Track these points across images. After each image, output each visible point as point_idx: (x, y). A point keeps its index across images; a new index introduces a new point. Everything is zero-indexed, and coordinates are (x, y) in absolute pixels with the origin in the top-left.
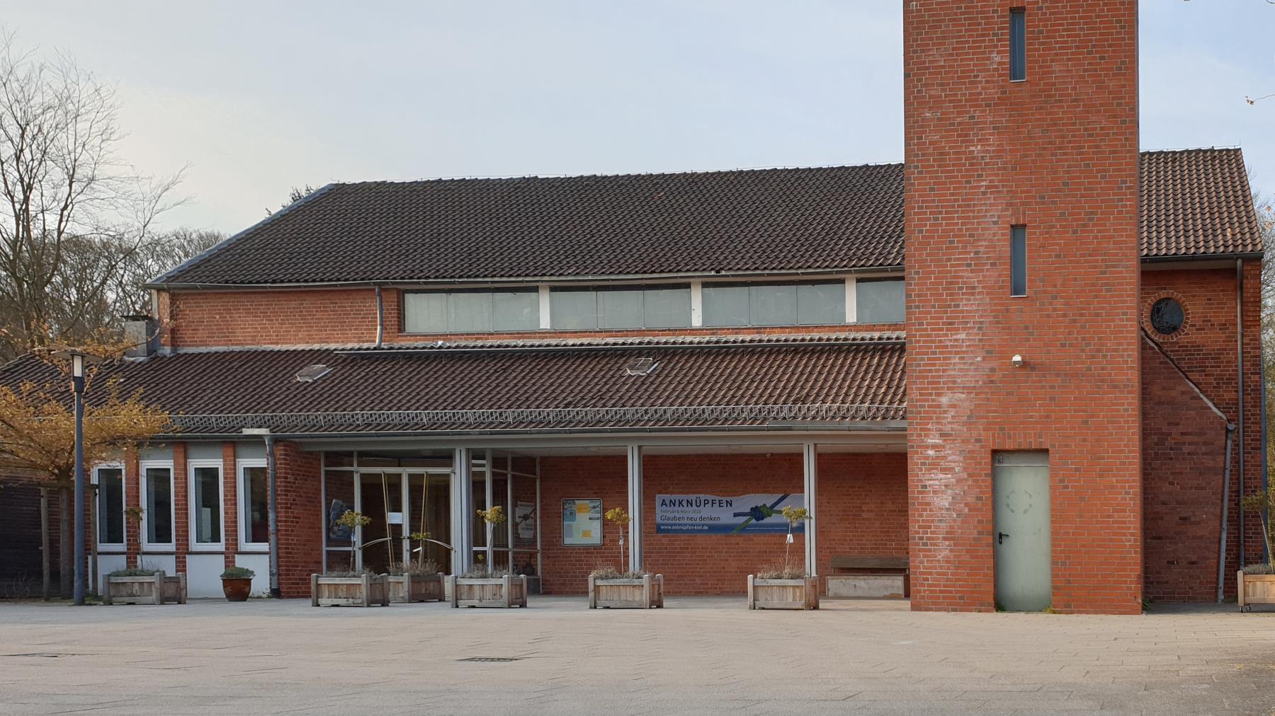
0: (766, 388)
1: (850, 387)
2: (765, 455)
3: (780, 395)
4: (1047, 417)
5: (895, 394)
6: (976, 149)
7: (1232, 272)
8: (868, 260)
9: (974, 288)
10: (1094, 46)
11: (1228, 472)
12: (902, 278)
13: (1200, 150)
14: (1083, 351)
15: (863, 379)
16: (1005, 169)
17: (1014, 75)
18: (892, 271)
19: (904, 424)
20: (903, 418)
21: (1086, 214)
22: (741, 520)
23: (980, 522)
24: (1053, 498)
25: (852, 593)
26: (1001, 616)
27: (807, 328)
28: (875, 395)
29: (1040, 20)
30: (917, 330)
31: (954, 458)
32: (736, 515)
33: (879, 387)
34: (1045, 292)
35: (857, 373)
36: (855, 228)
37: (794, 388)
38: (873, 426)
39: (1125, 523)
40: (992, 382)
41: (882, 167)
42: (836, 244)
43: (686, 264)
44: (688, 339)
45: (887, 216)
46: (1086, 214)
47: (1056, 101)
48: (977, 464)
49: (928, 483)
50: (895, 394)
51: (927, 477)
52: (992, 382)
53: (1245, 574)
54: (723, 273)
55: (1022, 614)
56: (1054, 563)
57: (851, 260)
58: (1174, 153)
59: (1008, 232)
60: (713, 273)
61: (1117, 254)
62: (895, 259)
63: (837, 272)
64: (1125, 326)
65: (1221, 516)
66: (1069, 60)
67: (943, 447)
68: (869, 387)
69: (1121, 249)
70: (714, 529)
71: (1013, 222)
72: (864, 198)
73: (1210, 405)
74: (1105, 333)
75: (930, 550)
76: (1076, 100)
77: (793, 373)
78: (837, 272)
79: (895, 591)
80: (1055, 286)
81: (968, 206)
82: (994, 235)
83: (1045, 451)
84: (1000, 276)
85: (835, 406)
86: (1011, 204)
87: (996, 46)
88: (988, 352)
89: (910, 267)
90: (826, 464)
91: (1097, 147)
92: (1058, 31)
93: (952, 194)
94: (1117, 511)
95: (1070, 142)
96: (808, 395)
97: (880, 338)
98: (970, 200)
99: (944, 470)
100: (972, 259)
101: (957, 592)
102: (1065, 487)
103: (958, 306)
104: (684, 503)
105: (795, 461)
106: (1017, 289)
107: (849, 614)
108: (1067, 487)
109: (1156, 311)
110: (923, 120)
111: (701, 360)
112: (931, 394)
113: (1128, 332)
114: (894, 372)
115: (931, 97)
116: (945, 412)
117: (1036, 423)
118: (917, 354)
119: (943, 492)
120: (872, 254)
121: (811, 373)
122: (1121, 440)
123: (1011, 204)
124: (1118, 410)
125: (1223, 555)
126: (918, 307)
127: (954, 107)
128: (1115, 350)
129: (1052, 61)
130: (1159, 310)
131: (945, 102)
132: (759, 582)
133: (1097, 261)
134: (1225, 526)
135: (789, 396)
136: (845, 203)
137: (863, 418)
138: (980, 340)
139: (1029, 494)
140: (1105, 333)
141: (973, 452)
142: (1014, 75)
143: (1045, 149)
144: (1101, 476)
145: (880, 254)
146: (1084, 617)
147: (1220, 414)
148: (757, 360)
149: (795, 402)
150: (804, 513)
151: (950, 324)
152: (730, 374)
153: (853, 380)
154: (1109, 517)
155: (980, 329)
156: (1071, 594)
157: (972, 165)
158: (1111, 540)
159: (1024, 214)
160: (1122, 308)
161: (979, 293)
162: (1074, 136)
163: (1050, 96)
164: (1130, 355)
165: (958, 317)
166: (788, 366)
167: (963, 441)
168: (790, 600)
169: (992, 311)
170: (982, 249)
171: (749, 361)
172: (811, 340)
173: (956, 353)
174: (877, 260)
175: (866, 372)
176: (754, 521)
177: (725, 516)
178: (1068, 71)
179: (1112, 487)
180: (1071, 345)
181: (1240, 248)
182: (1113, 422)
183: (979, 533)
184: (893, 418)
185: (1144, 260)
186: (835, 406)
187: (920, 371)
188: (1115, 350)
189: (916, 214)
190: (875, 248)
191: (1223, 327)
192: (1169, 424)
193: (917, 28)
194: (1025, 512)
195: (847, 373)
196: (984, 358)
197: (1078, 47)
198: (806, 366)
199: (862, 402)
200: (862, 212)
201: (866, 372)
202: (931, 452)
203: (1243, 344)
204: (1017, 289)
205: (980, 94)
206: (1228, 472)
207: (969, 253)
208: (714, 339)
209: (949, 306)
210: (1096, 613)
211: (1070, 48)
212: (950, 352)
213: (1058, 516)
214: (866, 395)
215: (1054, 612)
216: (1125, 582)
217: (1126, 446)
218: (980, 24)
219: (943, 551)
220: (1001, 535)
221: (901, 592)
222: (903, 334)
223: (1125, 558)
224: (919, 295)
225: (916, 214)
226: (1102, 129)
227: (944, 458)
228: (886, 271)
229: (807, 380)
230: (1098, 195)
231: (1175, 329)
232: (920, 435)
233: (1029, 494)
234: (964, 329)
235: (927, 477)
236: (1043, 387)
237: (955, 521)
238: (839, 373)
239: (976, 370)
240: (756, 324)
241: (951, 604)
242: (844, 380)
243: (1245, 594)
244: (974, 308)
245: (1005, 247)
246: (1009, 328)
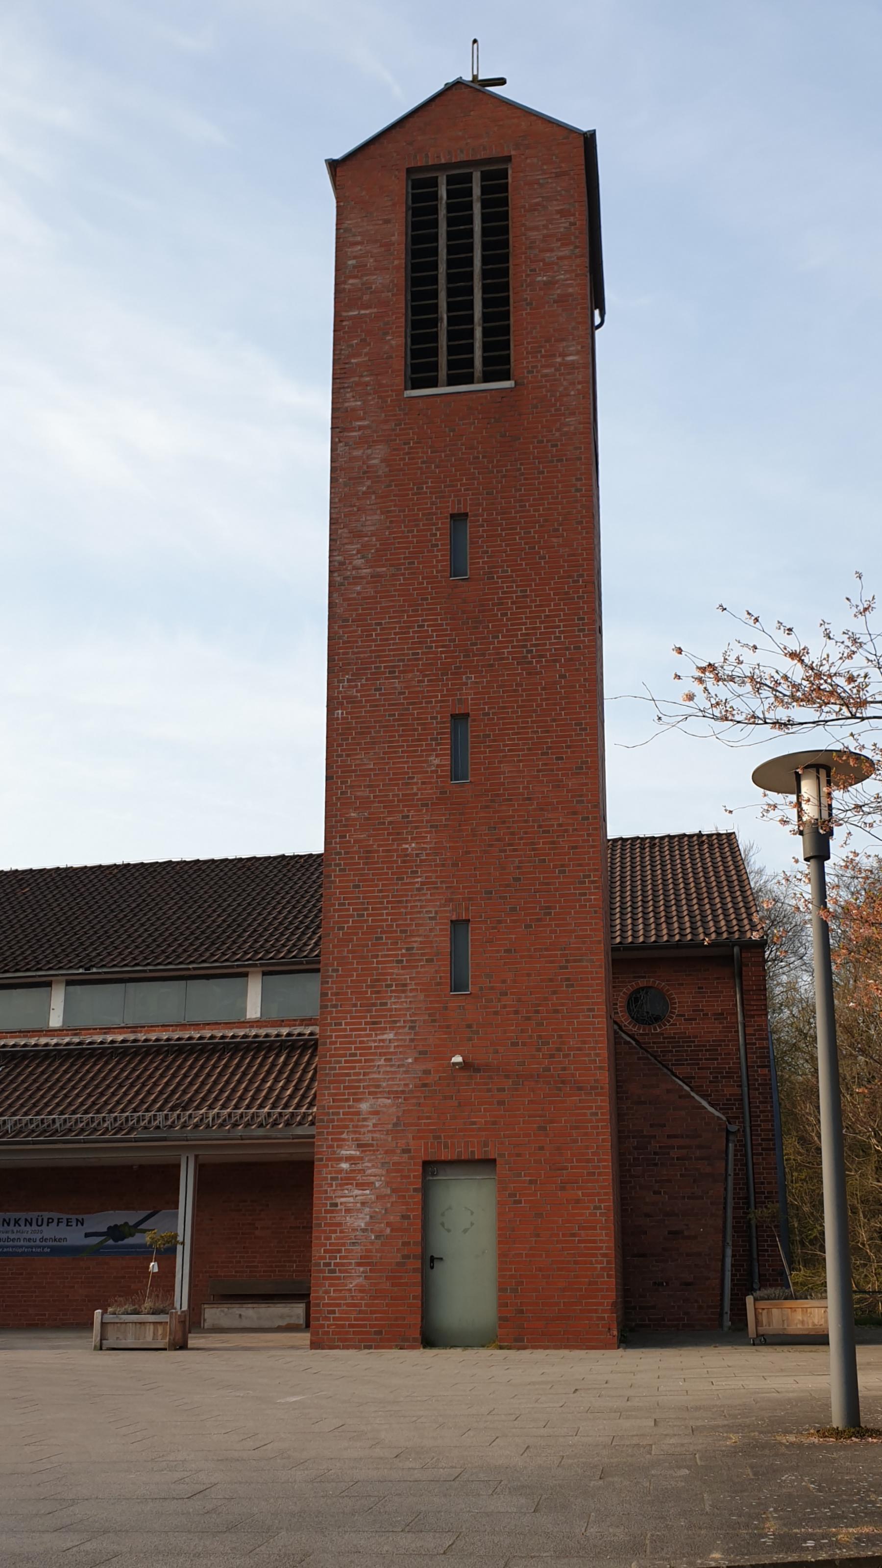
0: (137, 1093)
1: (246, 1090)
2: (131, 1167)
3: (155, 1101)
4: (495, 1123)
5: (304, 1097)
6: (411, 847)
7: (728, 959)
8: (279, 952)
9: (405, 985)
10: (548, 748)
11: (730, 1180)
12: (318, 971)
13: (684, 835)
14: (539, 1050)
15: (264, 1081)
16: (443, 865)
17: (455, 776)
18: (308, 963)
19: (313, 1131)
20: (312, 1123)
21: (541, 908)
22: (95, 1240)
23: (405, 1244)
24: (500, 1214)
25: (237, 1324)
26: (431, 1353)
27: (196, 1026)
28: (279, 1098)
29: (486, 725)
30: (332, 1031)
31: (373, 1170)
32: (87, 1235)
33: (284, 1088)
34: (492, 988)
35: (256, 1073)
36: (265, 919)
37: (173, 1092)
38: (274, 1134)
39: (594, 1242)
40: (425, 1085)
41: (301, 857)
42: (239, 936)
43: (49, 962)
44: (43, 1041)
45: (304, 906)
46: (541, 908)
47: (504, 800)
48: (403, 1177)
49: (339, 1201)
50: (304, 1097)
51: (339, 1193)
52: (425, 1085)
53: (756, 1300)
54: (94, 970)
55: (459, 1350)
56: (501, 1288)
57: (256, 953)
58: (653, 838)
59: (448, 927)
60: (81, 971)
61: (579, 949)
62: (312, 950)
63: (238, 966)
64: (593, 1023)
65: (725, 1227)
66: (520, 761)
67: (361, 1159)
68: (271, 1089)
69: (584, 943)
70: (56, 1251)
71: (454, 918)
72: (277, 888)
73: (704, 1103)
74: (567, 1030)
75: (339, 1278)
76: (529, 799)
77: (174, 1076)
78: (238, 966)
79: (293, 1321)
80: (504, 982)
81: (400, 902)
82: (431, 930)
83: (490, 1163)
84: (437, 972)
85: (226, 1112)
86: (451, 900)
87: (435, 750)
88: (420, 1053)
89: (327, 965)
90: (210, 1179)
91: (553, 843)
92: (508, 735)
93: (381, 891)
94: (584, 1228)
95: (521, 839)
96: (191, 1100)
97: (289, 1035)
98: (402, 896)
99: (361, 1186)
100: (403, 955)
101: (371, 1326)
102: (516, 1202)
103: (386, 1004)
104: (22, 1223)
105: (168, 1176)
106: (458, 984)
107: (227, 1355)
108: (520, 1202)
109: (634, 1000)
110: (347, 820)
111: (57, 1064)
112: (348, 1100)
113: (595, 1029)
114: (305, 1071)
115: (356, 798)
116: (365, 1120)
117: (480, 1129)
118: (331, 1056)
119: (359, 1211)
120: (284, 946)
121: (197, 1075)
122: (587, 1148)
123: (451, 900)
124: (585, 1115)
125: (728, 1275)
126: (335, 1006)
127: (385, 807)
128: (579, 1049)
129: (500, 762)
130: (636, 1000)
131: (373, 802)
132: (109, 1318)
133: (556, 955)
134: (729, 1240)
135: (166, 1101)
136: (254, 894)
137: (261, 1125)
138: (412, 1040)
139: (469, 1212)
140: (567, 1030)
141: (399, 1163)
142: (455, 776)
143: (491, 846)
144: (563, 1189)
145: (294, 945)
146: (540, 1354)
147: (717, 1113)
148: (129, 1062)
149: (173, 1109)
150: (176, 1236)
151: (374, 1023)
152: (93, 1079)
153: (251, 1081)
154: (574, 1235)
155: (411, 1028)
156: (522, 1324)
157: (404, 862)
158: (576, 1262)
159: (467, 909)
160: (588, 1004)
161: (411, 990)
162: (526, 833)
163: (498, 795)
164: (598, 1052)
165: (385, 1016)
166: (168, 1068)
167: (386, 1152)
168: (149, 1338)
169: (427, 1009)
170: (415, 945)
171: (118, 1063)
172: (201, 1038)
173: (381, 1054)
174: (289, 951)
175: (269, 1072)
176: (111, 1242)
177: (74, 1237)
178: (519, 772)
179: (578, 1201)
180: (524, 1044)
181: (737, 935)
182: (577, 1128)
183: (404, 1257)
184: (300, 1124)
185: (615, 949)
186: (226, 1112)
187: (335, 1075)
188: (579, 1049)
189: (335, 911)
190: (288, 940)
191: (719, 1016)
192: (651, 1126)
193: (341, 734)
194: (465, 1231)
195: (244, 1074)
196: (416, 1059)
197: (529, 749)
198: (191, 1067)
199: (261, 1106)
200: (274, 903)
201: (269, 1072)
202: (345, 1166)
203: (745, 1034)
204: (458, 984)
205: (416, 794)
206: (730, 1180)
207: (401, 949)
208: (76, 1040)
209: (374, 1005)
210: (557, 1347)
211: (523, 750)
212: (375, 1054)
213: (506, 1236)
214: (266, 1098)
215: (501, 1348)
216: (596, 1311)
217: (594, 1154)
218: (416, 730)
219: (356, 1279)
220: (432, 1259)
221: (302, 1321)
222: (316, 1029)
223: (596, 1283)
224: (337, 994)
225: (335, 911)
226: (560, 825)
227: (363, 1171)
228: (301, 963)
229: (191, 1084)
230: (556, 890)
231: (657, 1019)
232: (331, 1147)
233: (469, 1212)
234: (392, 1029)
235: (339, 1193)
236: (489, 1090)
237: (372, 1243)
238: (233, 1074)
239: (406, 1072)
240: (130, 1022)
241: (361, 1341)
242: (239, 1082)
243: (758, 1323)
244: (405, 1006)
245: (445, 943)
246: (448, 1027)
